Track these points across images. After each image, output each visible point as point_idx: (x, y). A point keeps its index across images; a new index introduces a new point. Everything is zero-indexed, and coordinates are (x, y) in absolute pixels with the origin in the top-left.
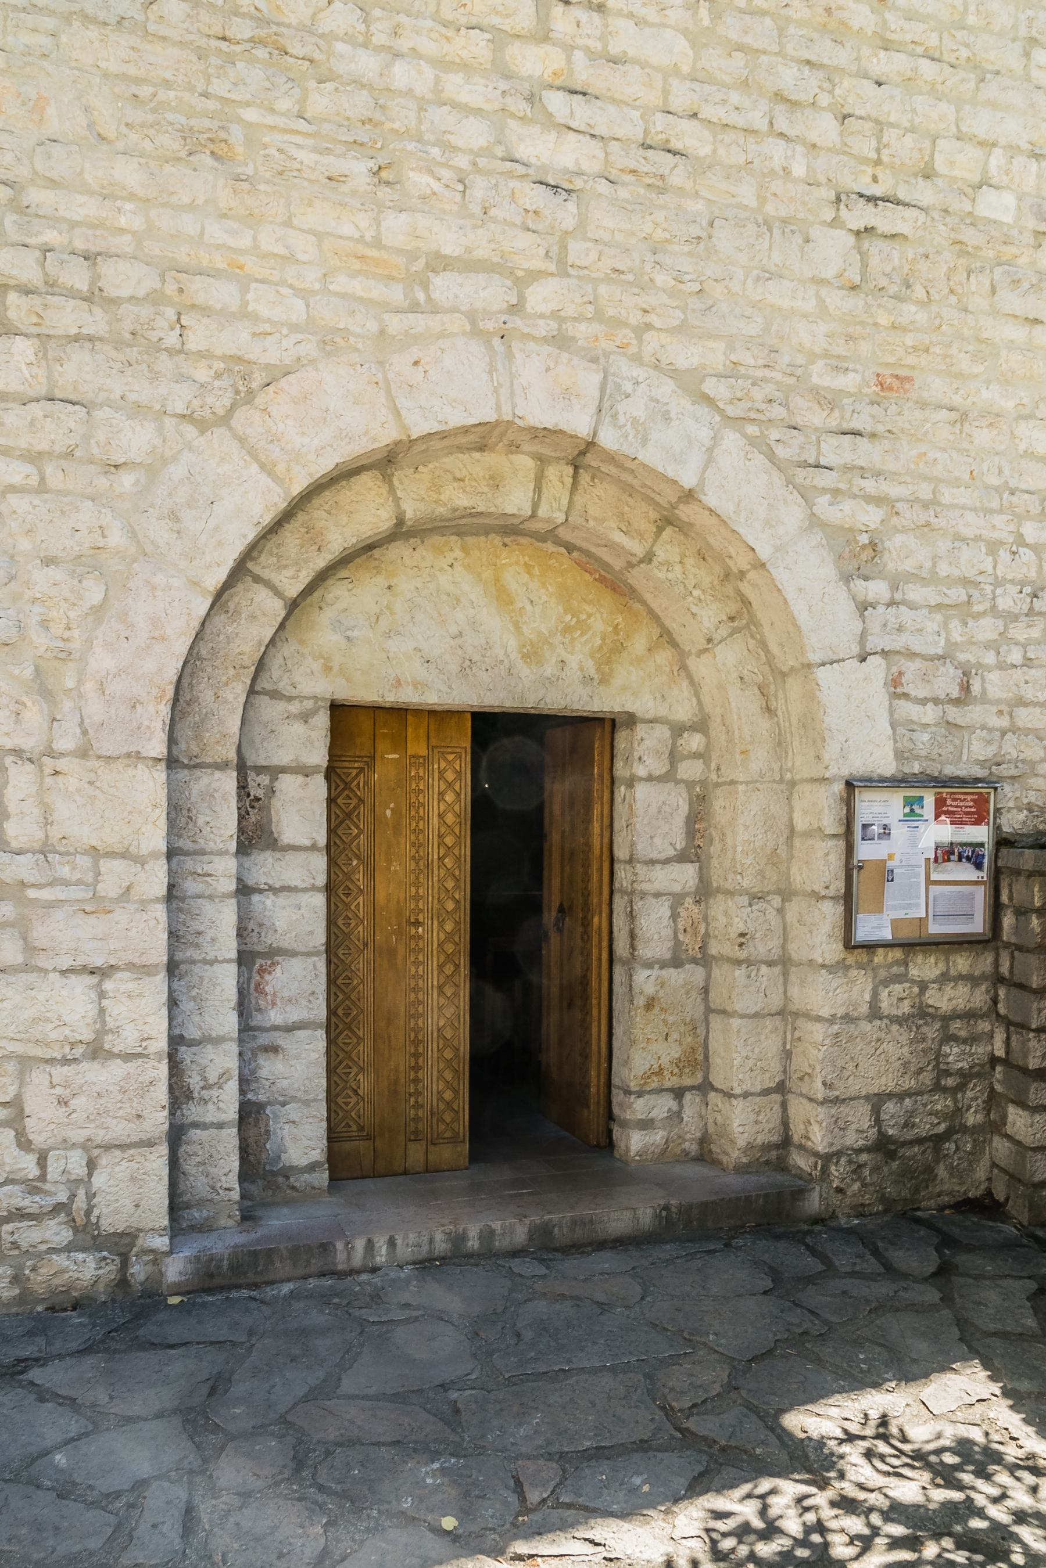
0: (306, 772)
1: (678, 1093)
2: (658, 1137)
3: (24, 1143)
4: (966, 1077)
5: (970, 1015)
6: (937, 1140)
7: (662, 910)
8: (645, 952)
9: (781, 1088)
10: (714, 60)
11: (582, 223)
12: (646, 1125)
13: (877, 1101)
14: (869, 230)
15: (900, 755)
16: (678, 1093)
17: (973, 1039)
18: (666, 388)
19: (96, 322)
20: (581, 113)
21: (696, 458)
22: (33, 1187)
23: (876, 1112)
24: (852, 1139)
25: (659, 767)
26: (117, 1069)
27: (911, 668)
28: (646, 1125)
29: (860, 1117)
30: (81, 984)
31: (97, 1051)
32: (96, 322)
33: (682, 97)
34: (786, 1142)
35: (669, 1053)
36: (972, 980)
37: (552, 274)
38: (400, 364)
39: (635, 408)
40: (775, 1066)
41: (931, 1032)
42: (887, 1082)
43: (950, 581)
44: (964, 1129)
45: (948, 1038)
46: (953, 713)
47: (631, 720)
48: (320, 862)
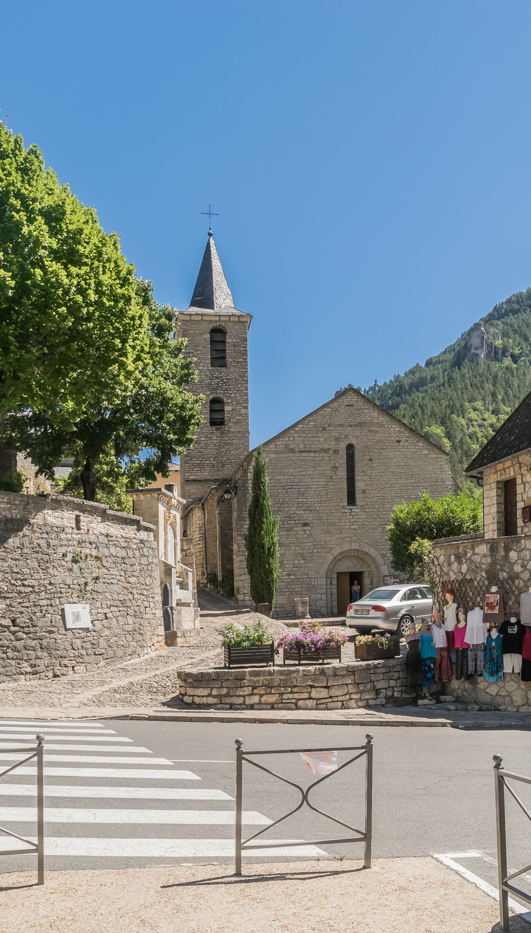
19: (320, 547)
20: (357, 523)
31: (321, 600)
32: (320, 547)
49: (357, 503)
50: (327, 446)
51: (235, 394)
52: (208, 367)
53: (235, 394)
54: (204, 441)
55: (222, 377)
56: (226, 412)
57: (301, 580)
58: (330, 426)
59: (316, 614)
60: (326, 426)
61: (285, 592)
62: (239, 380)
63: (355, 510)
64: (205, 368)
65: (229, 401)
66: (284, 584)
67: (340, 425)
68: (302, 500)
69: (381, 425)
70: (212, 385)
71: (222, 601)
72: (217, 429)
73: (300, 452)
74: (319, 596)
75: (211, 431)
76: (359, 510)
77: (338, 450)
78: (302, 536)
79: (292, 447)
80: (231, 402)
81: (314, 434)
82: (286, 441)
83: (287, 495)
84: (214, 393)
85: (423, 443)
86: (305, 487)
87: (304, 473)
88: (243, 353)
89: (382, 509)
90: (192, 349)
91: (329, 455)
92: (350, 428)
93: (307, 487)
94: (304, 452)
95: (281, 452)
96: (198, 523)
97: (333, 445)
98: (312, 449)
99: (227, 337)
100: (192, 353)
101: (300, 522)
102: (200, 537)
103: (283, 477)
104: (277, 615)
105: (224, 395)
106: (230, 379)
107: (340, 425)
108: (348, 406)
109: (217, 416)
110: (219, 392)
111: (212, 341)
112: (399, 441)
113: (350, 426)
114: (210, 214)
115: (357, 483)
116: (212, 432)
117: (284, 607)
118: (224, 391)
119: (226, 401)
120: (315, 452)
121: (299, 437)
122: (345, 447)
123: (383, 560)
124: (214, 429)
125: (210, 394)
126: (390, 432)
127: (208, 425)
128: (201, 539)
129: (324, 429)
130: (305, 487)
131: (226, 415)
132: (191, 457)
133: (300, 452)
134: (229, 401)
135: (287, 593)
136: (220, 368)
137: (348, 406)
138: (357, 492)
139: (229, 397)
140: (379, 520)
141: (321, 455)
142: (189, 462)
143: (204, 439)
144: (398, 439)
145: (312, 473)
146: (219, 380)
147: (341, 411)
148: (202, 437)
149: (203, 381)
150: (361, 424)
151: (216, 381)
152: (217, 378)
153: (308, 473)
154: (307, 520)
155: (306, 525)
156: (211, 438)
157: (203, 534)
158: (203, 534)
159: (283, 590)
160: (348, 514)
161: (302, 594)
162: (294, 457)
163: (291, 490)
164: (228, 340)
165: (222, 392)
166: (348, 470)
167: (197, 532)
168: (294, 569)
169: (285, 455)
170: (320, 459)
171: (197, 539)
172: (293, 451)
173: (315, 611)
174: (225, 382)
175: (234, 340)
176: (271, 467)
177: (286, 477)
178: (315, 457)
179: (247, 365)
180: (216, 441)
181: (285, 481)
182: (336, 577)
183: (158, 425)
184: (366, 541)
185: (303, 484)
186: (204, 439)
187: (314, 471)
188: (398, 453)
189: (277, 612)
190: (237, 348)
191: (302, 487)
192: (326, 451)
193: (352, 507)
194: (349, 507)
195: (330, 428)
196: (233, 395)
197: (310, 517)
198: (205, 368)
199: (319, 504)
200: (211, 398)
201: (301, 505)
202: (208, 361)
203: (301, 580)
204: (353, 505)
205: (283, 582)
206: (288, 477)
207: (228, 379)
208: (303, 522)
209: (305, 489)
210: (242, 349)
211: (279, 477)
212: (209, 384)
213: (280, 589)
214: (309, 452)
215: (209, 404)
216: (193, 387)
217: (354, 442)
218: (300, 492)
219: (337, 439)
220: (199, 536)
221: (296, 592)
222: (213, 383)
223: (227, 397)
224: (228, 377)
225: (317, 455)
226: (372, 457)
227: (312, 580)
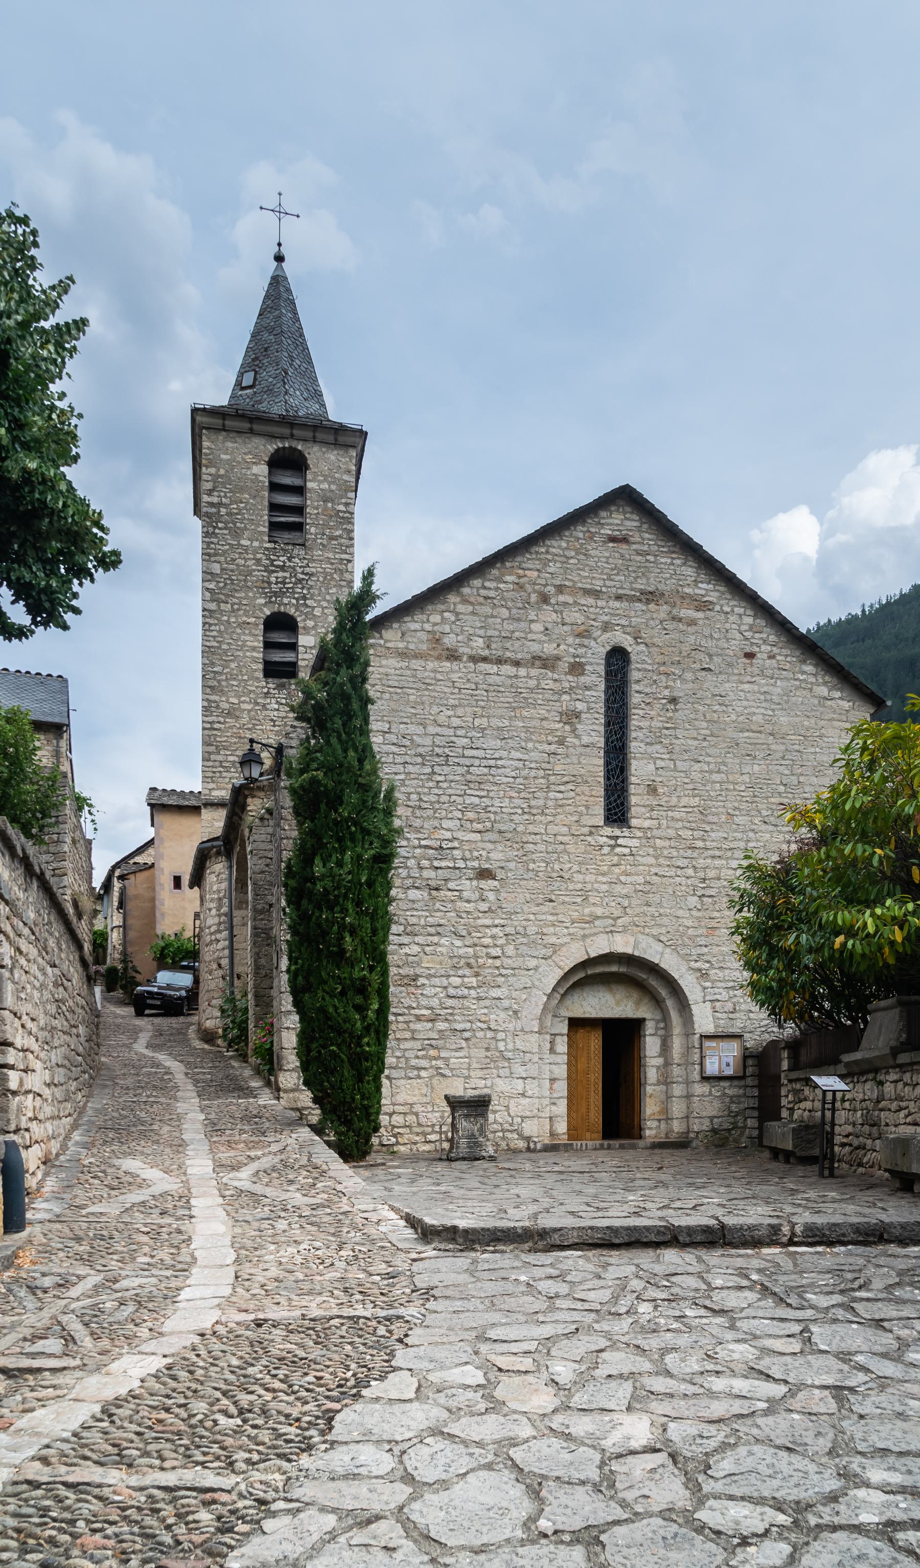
0: (562, 1035)
1: (659, 1120)
2: (654, 1132)
3: (509, 1115)
4: (737, 1114)
5: (739, 1096)
6: (729, 1130)
7: (654, 1070)
8: (649, 1082)
9: (687, 1117)
10: (662, 861)
11: (630, 904)
12: (650, 1129)
13: (711, 1118)
14: (703, 895)
15: (716, 1026)
16: (659, 1120)
17: (739, 1103)
18: (651, 940)
19: (525, 940)
20: (630, 879)
21: (658, 957)
22: (511, 1125)
23: (711, 1121)
24: (704, 1128)
25: (653, 1032)
26: (528, 1100)
27: (718, 1004)
28: (650, 1129)
29: (707, 1122)
30: (520, 1081)
31: (523, 1095)
32: (525, 940)
33: (654, 870)
34: (688, 1132)
35: (656, 1109)
36: (740, 1087)
37: (710, 1529)
38: (588, 941)
39: (644, 945)
40: (685, 1111)
41: (727, 1100)
42: (714, 1113)
43: (729, 981)
44: (737, 1127)
45: (733, 1102)
46: (731, 1016)
47: (644, 1020)
48: (566, 1057)
49: (634, 822)
50: (549, 649)
51: (323, 608)
52: (262, 541)
53: (323, 608)
54: (249, 711)
55: (294, 568)
56: (301, 649)
57: (467, 1035)
58: (560, 589)
59: (509, 1135)
60: (551, 590)
61: (419, 1069)
62: (333, 578)
63: (628, 840)
64: (256, 544)
65: (310, 623)
66: (418, 1045)
67: (588, 592)
68: (476, 800)
69: (703, 605)
70: (269, 583)
71: (241, 1089)
72: (280, 687)
73: (474, 659)
74: (519, 1085)
75: (265, 690)
76: (635, 843)
77: (581, 665)
78: (470, 907)
79: (449, 641)
80: (314, 628)
81: (514, 611)
82: (435, 624)
83: (431, 784)
84: (275, 602)
85: (816, 666)
86: (485, 763)
87: (484, 722)
88: (343, 518)
89: (700, 844)
90: (225, 496)
91: (556, 676)
92: (617, 604)
93: (492, 762)
94: (485, 659)
95: (417, 656)
96: (215, 888)
97: (568, 649)
98: (508, 654)
99: (309, 477)
100: (226, 506)
101: (469, 864)
102: (220, 923)
103: (419, 730)
104: (395, 1136)
105: (297, 610)
106: (312, 575)
107: (588, 592)
108: (613, 539)
109: (279, 656)
110: (286, 601)
111: (274, 487)
112: (750, 656)
113: (619, 598)
114: (280, 212)
115: (633, 762)
116: (268, 693)
117: (417, 1114)
118: (297, 599)
119: (300, 625)
120: (517, 664)
121: (473, 613)
122: (603, 651)
123: (699, 988)
124: (271, 685)
125: (265, 605)
126: (728, 626)
127: (260, 675)
128: (222, 927)
129: (545, 599)
130: (485, 763)
131: (300, 656)
132: (217, 747)
133: (474, 659)
134: (310, 623)
135: (423, 1074)
136: (290, 547)
137: (613, 539)
138: (632, 789)
139: (307, 616)
140: (690, 872)
141: (534, 672)
142: (213, 757)
143: (249, 707)
144: (748, 650)
145: (507, 723)
146: (287, 575)
147: (592, 552)
148: (244, 702)
149: (250, 574)
150: (650, 597)
151: (280, 574)
152: (283, 568)
153: (495, 722)
154: (488, 859)
155: (484, 874)
156: (264, 705)
157: (225, 915)
158: (225, 915)
159: (414, 1062)
160: (606, 850)
161: (469, 1077)
162: (457, 671)
163: (446, 769)
164: (310, 485)
165: (294, 601)
166: (608, 724)
167: (214, 912)
168: (450, 1002)
169: (431, 665)
170: (532, 683)
171: (213, 929)
172: (453, 656)
173: (506, 1126)
174: (300, 581)
175: (325, 486)
176: (387, 696)
177: (432, 729)
178: (516, 676)
179: (352, 546)
180: (276, 713)
181: (428, 741)
182: (565, 1031)
183: (21, 508)
184: (655, 931)
185: (480, 753)
186: (249, 707)
187: (510, 718)
188: (746, 687)
189: (394, 1127)
190: (330, 505)
191: (477, 762)
192: (547, 663)
193: (617, 832)
194: (608, 831)
195: (562, 598)
196: (318, 612)
197: (497, 856)
198: (256, 544)
199: (526, 817)
200: (268, 613)
201: (471, 815)
202: (261, 529)
203: (467, 1035)
204: (620, 827)
205: (413, 1039)
206: (438, 730)
207: (306, 574)
208: (476, 864)
209: (486, 770)
210: (342, 508)
211: (412, 729)
212: (263, 581)
213: (407, 1059)
214: (500, 661)
215: (262, 627)
216: (226, 584)
217: (627, 642)
218: (469, 777)
219: (584, 634)
220: (216, 920)
221: (452, 1070)
222: (273, 579)
223: (306, 614)
224: (307, 570)
225: (522, 672)
226: (676, 694)
227: (501, 1036)
